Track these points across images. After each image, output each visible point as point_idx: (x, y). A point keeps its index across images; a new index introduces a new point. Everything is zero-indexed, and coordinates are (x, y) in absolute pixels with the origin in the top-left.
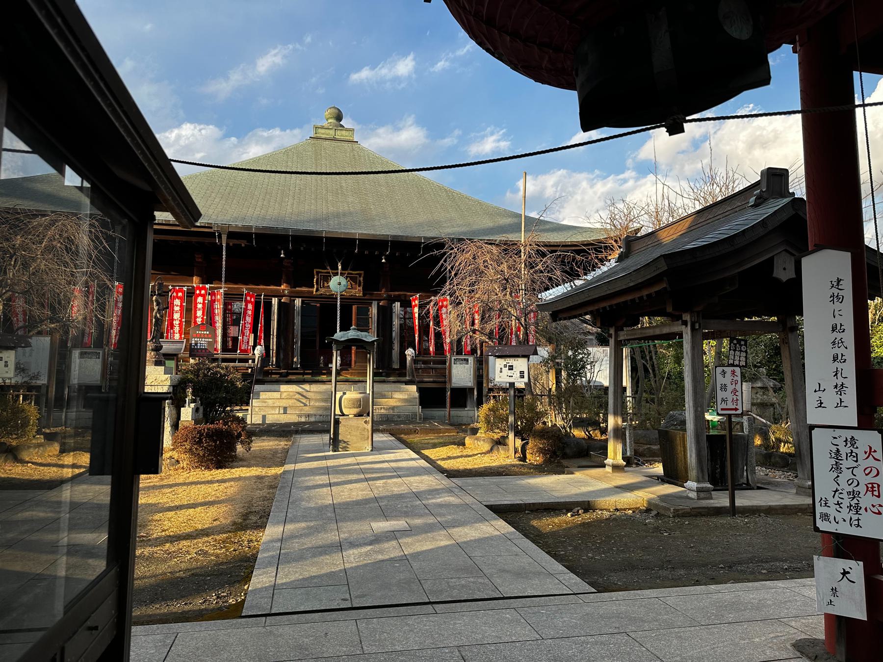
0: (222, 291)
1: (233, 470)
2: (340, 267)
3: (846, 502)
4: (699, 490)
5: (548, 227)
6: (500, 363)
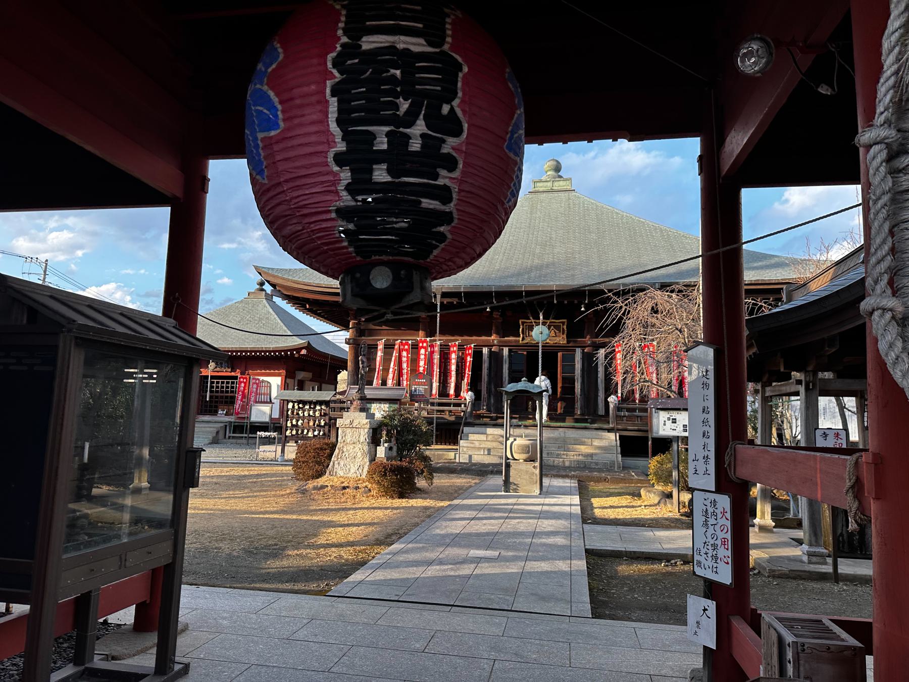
1: (410, 501)
3: (710, 553)
4: (810, 554)
5: (773, 261)
6: (663, 415)
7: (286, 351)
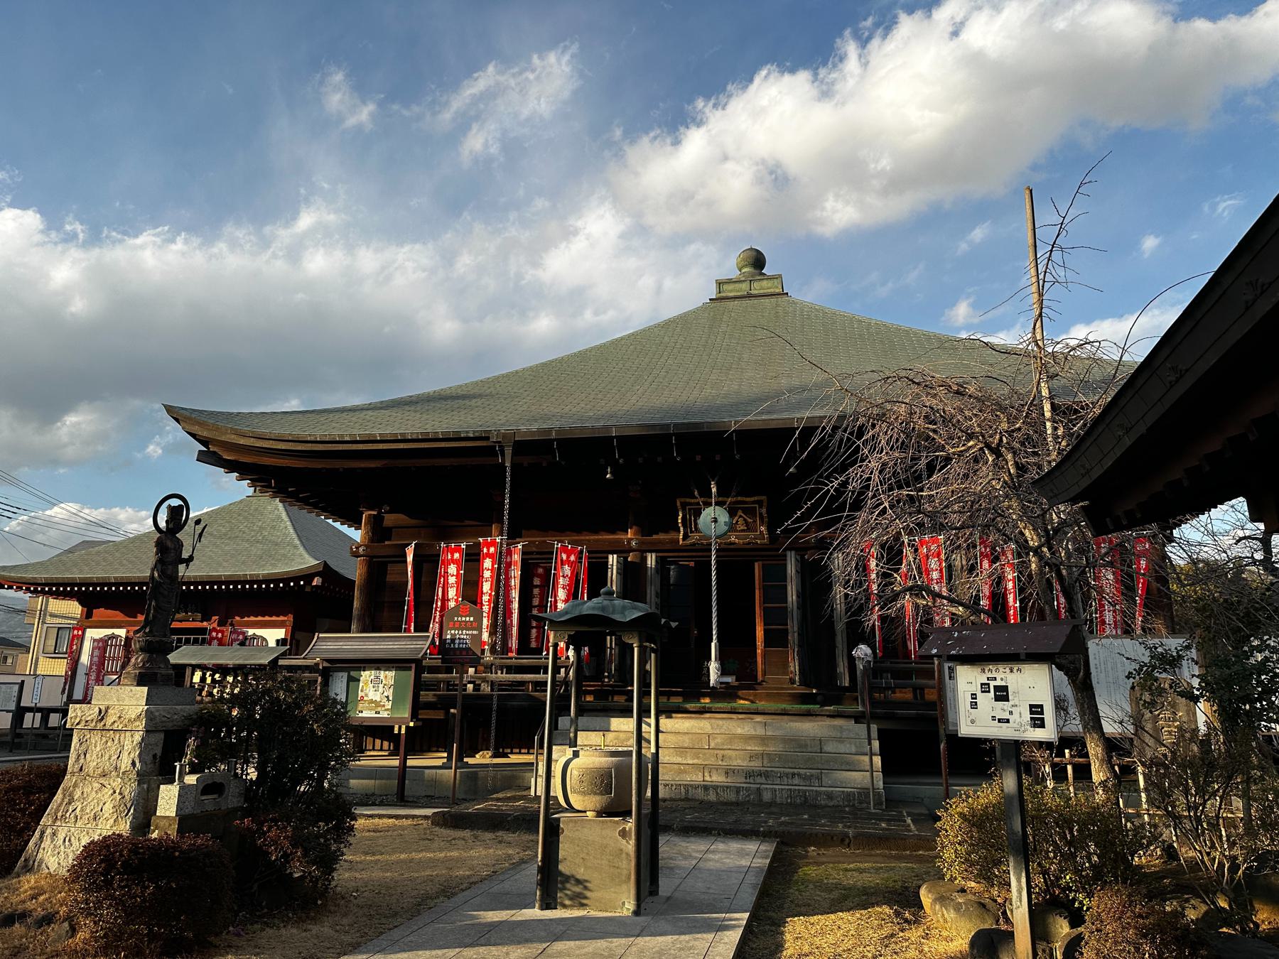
0: (520, 547)
2: (714, 490)
6: (967, 680)
7: (286, 581)
